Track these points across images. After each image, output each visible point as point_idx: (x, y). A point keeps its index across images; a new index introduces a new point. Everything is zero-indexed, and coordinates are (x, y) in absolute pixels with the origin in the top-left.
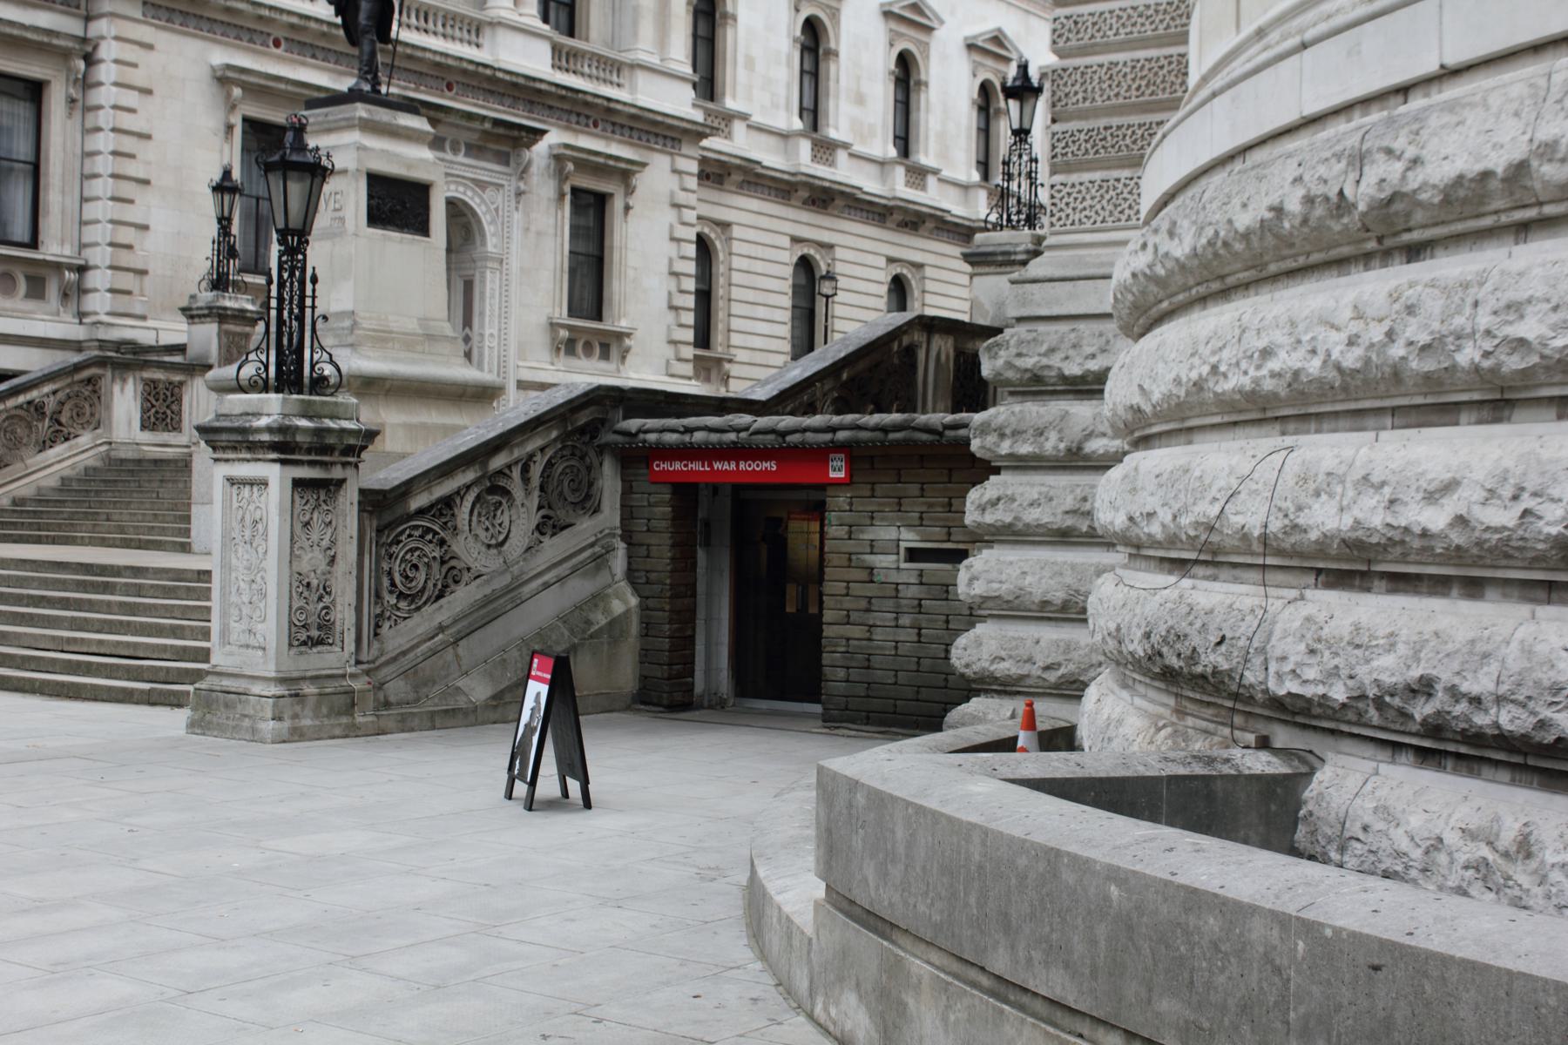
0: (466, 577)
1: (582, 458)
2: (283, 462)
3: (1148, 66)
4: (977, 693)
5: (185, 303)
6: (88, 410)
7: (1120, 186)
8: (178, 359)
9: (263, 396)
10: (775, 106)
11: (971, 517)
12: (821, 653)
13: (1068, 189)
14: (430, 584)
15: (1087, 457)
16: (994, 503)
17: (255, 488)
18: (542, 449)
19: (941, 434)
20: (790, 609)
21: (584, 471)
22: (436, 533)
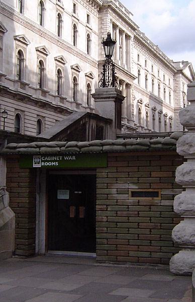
4: (181, 249)
11: (178, 178)
12: (95, 233)
16: (188, 173)
19: (149, 146)
20: (72, 215)
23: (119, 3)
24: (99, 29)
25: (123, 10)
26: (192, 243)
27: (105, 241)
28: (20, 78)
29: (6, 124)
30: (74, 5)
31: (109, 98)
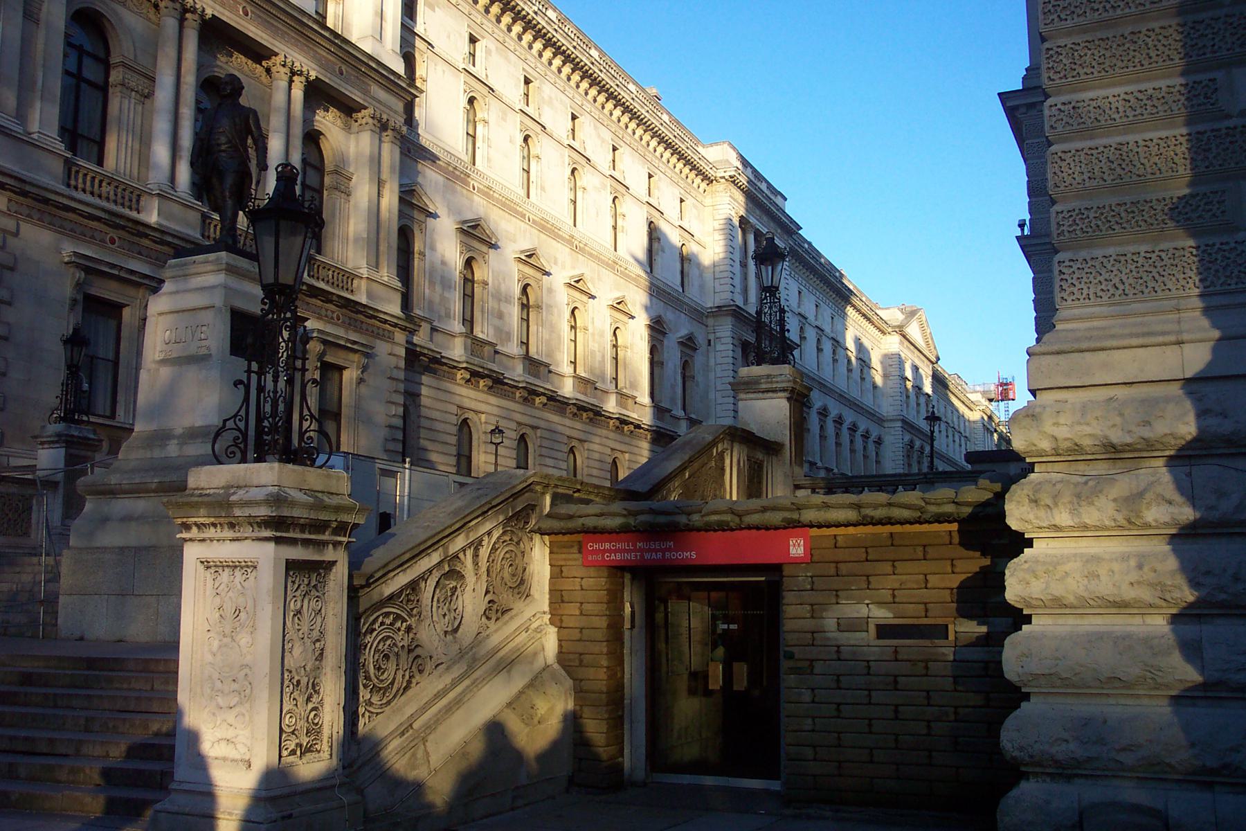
0: (429, 666)
1: (518, 543)
2: (278, 541)
7: (1141, 260)
9: (242, 466)
14: (399, 677)
17: (238, 572)
18: (489, 533)
21: (519, 554)
22: (404, 620)
25: (763, 187)
26: (1056, 762)
27: (809, 752)
31: (774, 391)
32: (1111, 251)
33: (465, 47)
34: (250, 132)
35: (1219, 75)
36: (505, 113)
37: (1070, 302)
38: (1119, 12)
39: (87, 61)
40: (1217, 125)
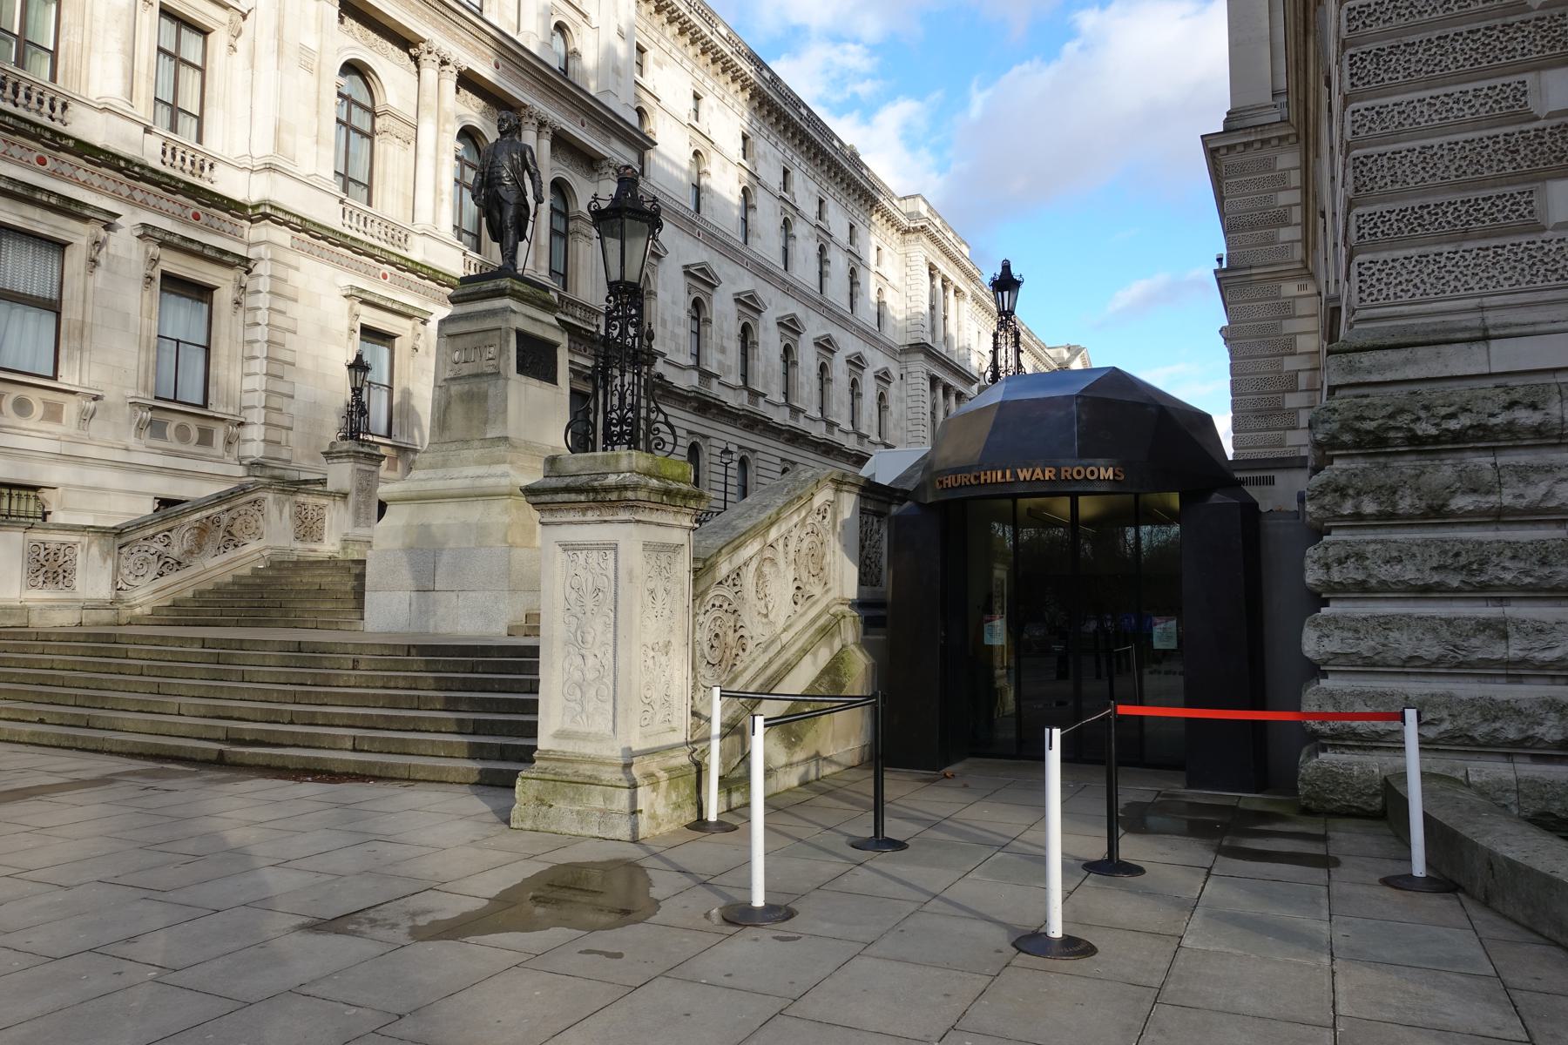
3: (1468, 147)
5: (326, 449)
6: (253, 524)
7: (1443, 260)
8: (320, 488)
10: (678, 350)
13: (1379, 266)
15: (1452, 514)
23: (943, 222)
24: (901, 279)
26: (1356, 734)
28: (745, 382)
29: (722, 479)
30: (852, 227)
32: (1412, 252)
33: (691, 104)
34: (526, 167)
35: (1529, 78)
36: (725, 166)
37: (1369, 302)
38: (1426, 16)
39: (355, 110)
40: (1525, 127)
